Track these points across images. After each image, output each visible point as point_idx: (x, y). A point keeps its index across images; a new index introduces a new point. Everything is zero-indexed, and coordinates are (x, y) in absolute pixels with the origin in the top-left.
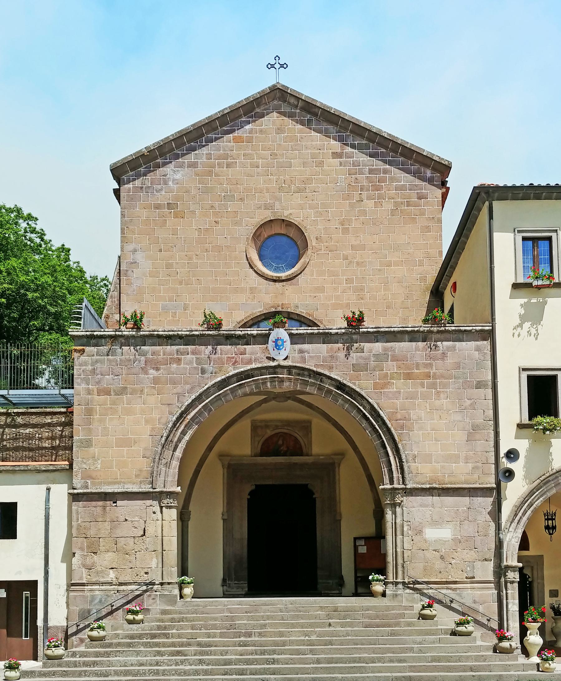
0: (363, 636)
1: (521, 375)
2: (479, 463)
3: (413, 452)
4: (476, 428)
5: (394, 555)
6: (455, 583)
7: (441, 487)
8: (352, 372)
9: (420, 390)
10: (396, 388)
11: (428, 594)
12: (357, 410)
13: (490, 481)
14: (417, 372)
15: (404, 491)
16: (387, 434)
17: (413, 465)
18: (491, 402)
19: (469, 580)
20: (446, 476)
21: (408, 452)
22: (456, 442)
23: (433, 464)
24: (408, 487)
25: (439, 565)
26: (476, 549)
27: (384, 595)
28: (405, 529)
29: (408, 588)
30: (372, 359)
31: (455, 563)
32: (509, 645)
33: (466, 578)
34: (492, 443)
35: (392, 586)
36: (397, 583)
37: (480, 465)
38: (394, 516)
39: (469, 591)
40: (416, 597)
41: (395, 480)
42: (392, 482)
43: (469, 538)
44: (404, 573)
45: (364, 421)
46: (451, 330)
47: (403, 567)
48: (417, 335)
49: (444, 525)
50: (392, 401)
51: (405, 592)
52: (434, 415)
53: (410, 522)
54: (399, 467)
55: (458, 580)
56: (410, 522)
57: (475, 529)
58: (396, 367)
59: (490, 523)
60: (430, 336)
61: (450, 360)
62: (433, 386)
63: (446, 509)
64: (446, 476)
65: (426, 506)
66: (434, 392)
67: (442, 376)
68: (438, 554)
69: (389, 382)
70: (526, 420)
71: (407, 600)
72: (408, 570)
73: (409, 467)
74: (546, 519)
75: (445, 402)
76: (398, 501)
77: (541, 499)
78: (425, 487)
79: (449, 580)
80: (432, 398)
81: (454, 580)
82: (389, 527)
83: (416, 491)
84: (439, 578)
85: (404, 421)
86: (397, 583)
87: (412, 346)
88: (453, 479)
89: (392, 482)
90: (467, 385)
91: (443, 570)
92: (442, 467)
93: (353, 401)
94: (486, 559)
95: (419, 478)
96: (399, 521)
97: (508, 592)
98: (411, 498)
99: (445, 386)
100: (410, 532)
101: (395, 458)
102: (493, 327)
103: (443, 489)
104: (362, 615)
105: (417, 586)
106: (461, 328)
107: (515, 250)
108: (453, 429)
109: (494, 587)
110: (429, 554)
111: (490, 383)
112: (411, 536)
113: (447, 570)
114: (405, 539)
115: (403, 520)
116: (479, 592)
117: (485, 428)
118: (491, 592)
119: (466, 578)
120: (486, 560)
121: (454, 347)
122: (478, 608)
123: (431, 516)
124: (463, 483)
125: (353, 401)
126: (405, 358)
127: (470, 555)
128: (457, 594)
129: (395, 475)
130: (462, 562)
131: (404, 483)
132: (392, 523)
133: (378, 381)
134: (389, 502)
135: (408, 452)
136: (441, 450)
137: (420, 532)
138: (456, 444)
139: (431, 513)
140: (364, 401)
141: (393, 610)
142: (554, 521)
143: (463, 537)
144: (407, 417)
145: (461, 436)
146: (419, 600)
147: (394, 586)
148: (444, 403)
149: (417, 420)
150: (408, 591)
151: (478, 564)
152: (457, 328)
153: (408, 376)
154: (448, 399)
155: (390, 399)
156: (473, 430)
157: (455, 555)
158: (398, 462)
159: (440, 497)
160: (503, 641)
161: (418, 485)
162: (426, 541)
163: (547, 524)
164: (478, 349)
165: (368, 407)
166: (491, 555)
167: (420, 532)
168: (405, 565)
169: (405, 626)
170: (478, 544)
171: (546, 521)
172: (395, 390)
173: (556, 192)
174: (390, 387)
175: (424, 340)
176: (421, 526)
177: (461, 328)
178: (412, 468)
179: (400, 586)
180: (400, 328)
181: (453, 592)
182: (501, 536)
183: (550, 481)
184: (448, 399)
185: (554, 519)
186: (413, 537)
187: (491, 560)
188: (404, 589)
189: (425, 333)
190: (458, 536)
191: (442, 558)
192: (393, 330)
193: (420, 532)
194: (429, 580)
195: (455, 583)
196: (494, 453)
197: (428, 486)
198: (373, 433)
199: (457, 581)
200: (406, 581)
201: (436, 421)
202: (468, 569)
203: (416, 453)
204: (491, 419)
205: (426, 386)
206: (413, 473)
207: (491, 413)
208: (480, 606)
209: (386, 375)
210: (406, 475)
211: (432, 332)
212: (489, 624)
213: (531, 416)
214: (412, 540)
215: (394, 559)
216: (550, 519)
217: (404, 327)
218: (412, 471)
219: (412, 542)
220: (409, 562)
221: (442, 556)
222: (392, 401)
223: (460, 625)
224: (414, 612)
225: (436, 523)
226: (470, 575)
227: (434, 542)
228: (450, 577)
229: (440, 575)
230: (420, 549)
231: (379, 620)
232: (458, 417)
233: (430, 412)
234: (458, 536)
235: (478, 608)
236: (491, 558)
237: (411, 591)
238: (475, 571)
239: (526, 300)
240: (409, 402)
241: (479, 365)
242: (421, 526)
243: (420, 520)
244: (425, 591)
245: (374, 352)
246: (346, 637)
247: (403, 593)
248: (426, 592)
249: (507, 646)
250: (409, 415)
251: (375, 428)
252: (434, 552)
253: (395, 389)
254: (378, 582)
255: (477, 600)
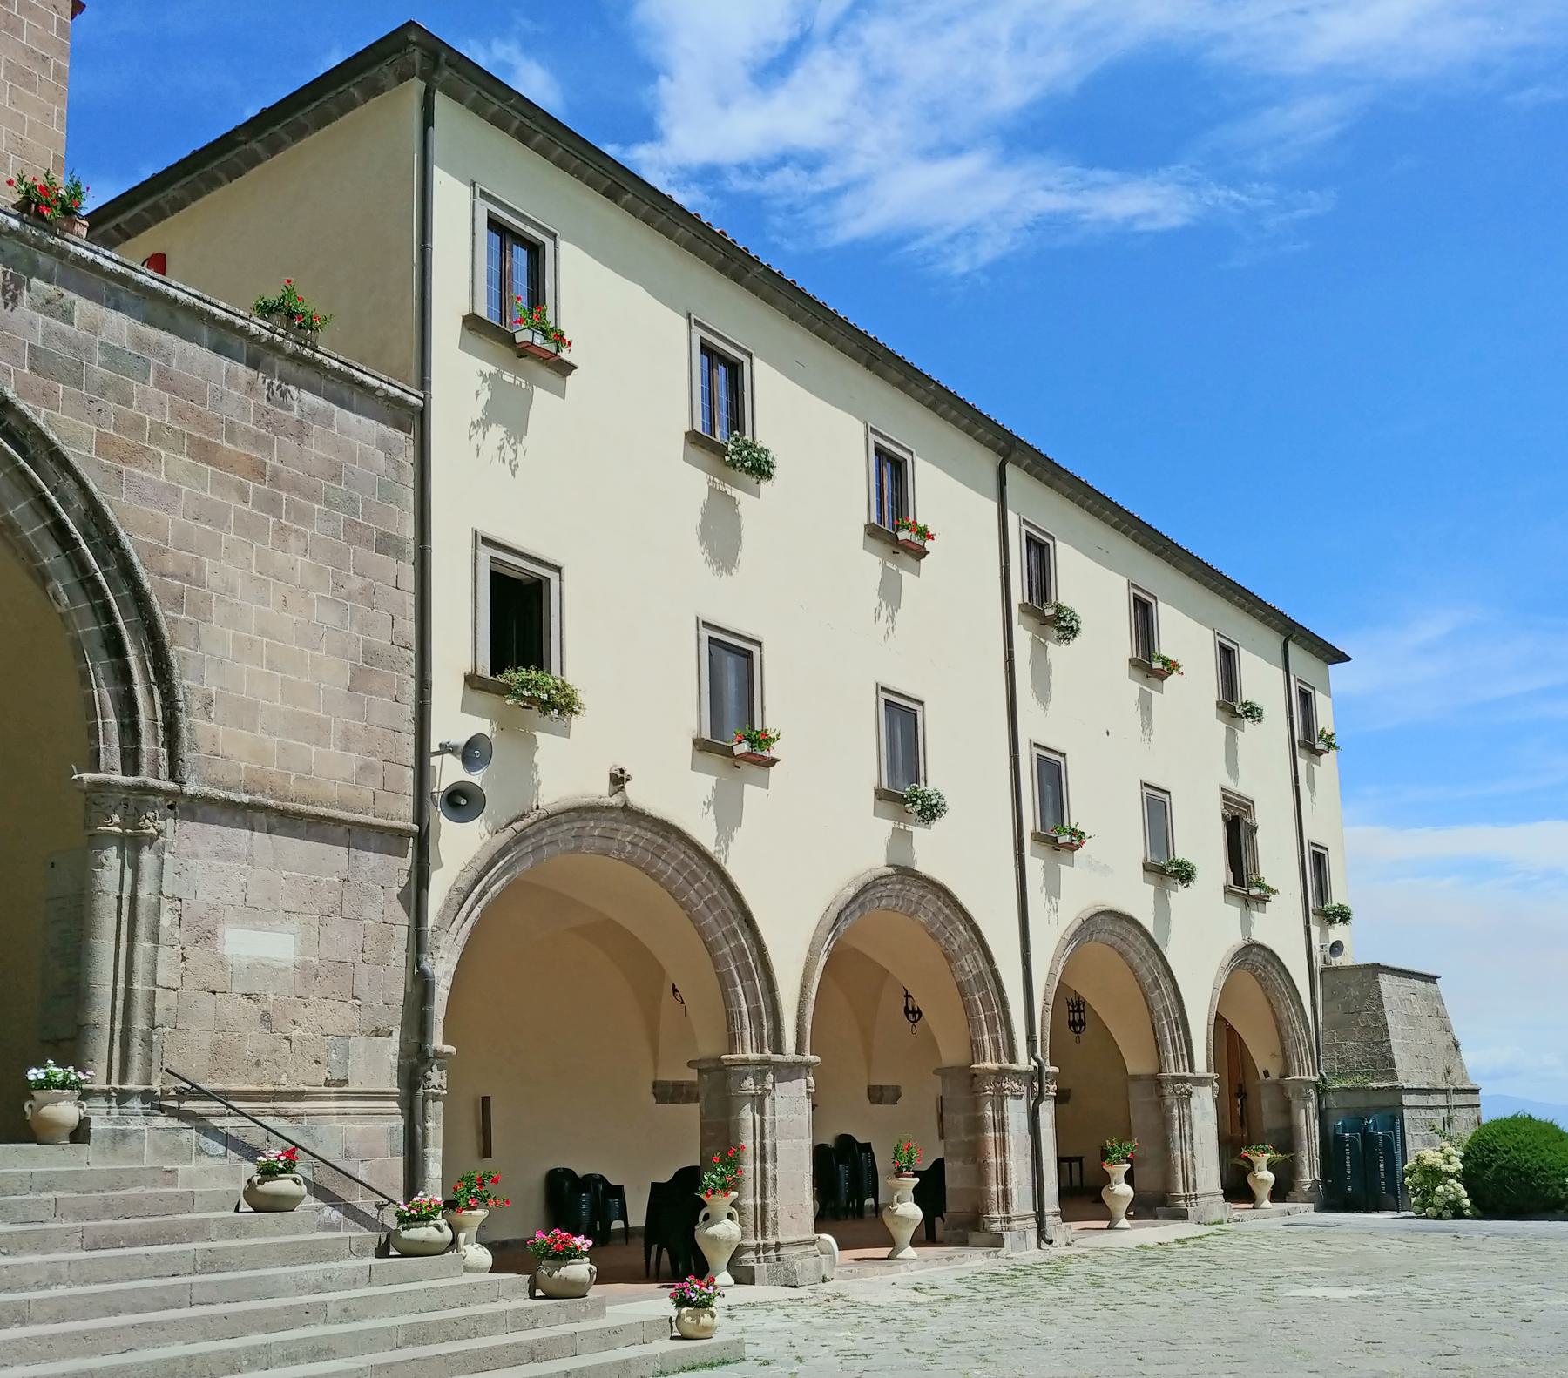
0: (110, 1281)
1: (478, 552)
2: (376, 756)
3: (205, 686)
4: (371, 656)
5: (119, 1003)
6: (298, 1096)
7: (281, 808)
8: (26, 370)
9: (234, 504)
10: (166, 475)
11: (221, 1130)
12: (30, 503)
13: (402, 813)
14: (230, 451)
15: (170, 802)
16: (133, 609)
17: (199, 722)
18: (410, 600)
19: (334, 1089)
20: (293, 778)
21: (190, 683)
22: (323, 685)
23: (258, 735)
24: (190, 789)
25: (255, 1040)
26: (357, 1001)
27: (80, 1134)
28: (166, 920)
29: (162, 1109)
30: (99, 356)
31: (302, 1039)
32: (588, 1273)
33: (328, 1083)
34: (409, 709)
35: (106, 1105)
36: (123, 1097)
37: (376, 761)
38: (128, 873)
39: (335, 1123)
40: (184, 1140)
41: (145, 761)
42: (131, 762)
43: (341, 966)
44: (148, 1062)
45: (54, 549)
46: (328, 366)
47: (148, 1042)
48: (235, 341)
49: (278, 922)
50: (154, 511)
51: (154, 1125)
52: (269, 590)
53: (180, 900)
54: (160, 723)
55: (307, 1089)
56: (180, 900)
57: (357, 943)
58: (170, 411)
59: (395, 930)
60: (269, 359)
61: (315, 450)
62: (272, 505)
63: (285, 873)
64: (293, 778)
65: (232, 857)
66: (271, 523)
67: (295, 487)
68: (255, 1006)
69: (147, 448)
70: (485, 669)
71: (157, 1150)
72: (165, 1055)
73: (190, 728)
74: (1070, 1011)
75: (299, 563)
76: (152, 830)
77: (504, 879)
78: (238, 800)
79: (283, 1088)
80: (268, 540)
81: (294, 1088)
82: (106, 910)
83: (206, 808)
84: (252, 1080)
85: (186, 585)
86: (123, 1097)
87: (219, 365)
88: (307, 789)
89: (131, 762)
90: (353, 531)
91: (266, 1056)
92: (284, 748)
93: (28, 468)
94: (377, 1030)
95: (217, 770)
96: (144, 893)
97: (428, 1125)
98: (189, 827)
99: (303, 516)
100: (177, 934)
101: (150, 692)
102: (426, 400)
103: (283, 813)
104: (52, 1207)
105: (188, 1105)
106: (356, 373)
107: (474, 234)
108: (317, 646)
109: (400, 1111)
110: (231, 1007)
111: (410, 548)
112: (179, 946)
113: (278, 1056)
114: (164, 953)
115: (161, 893)
116: (359, 1126)
117: (393, 665)
118: (388, 1125)
119: (328, 1083)
120: (377, 1033)
121: (327, 421)
122: (355, 1171)
123: (244, 888)
124: (332, 805)
125: (28, 468)
126: (194, 394)
127: (341, 1016)
128: (301, 1130)
129: (146, 745)
130: (319, 1035)
131: (173, 775)
132: (119, 898)
133: (112, 432)
134: (116, 829)
135: (190, 683)
136: (283, 698)
137: (207, 936)
138: (321, 692)
139: (243, 880)
140: (65, 479)
141: (135, 1183)
142: (1082, 1014)
143: (324, 962)
144: (194, 574)
145: (334, 673)
146: (194, 1150)
147: (114, 1104)
148: (297, 564)
149: (223, 592)
150: (161, 1121)
151: (359, 1044)
152: (344, 368)
153: (203, 451)
154: (308, 556)
155: (144, 499)
156: (367, 664)
157: (302, 1013)
158: (158, 706)
159: (273, 836)
160: (572, 1261)
161: (216, 791)
162: (222, 964)
163: (1071, 1019)
164: (384, 445)
165: (78, 503)
166: (394, 1019)
167: (209, 935)
168: (155, 1037)
169: (220, 1237)
170: (362, 986)
171: (1071, 1014)
172: (163, 478)
173: (564, 149)
174: (150, 465)
175: (253, 364)
176: (212, 918)
177: (356, 373)
178: (199, 734)
179: (136, 1104)
180: (195, 300)
181: (291, 1125)
182: (426, 965)
183: (528, 837)
184: (308, 556)
185: (1083, 1011)
186: (188, 948)
187: (391, 1034)
188: (146, 1114)
189: (259, 343)
190: (312, 959)
191: (266, 1019)
192: (173, 295)
193: (209, 935)
194: (226, 1087)
195: (298, 1096)
196: (413, 737)
197: (246, 799)
198: (79, 593)
199: (303, 1093)
200: (156, 1086)
201: (271, 609)
202: (334, 1056)
203: (214, 693)
204: (408, 645)
205: (251, 498)
206: (202, 750)
207: (409, 628)
208: (360, 1165)
209: (138, 425)
210: (187, 755)
211: (276, 348)
212: (381, 1218)
213: (497, 666)
214: (184, 959)
215: (119, 1014)
216: (1076, 1011)
217: (205, 301)
218: (200, 743)
219: (182, 965)
220: (168, 1029)
221: (266, 1013)
222: (154, 511)
223: (418, 1224)
224: (179, 1189)
225: (254, 913)
226: (338, 1075)
227: (246, 971)
228: (283, 1080)
229: (256, 1072)
230: (204, 989)
231: (110, 1222)
232: (331, 617)
233: (259, 578)
234: (312, 959)
235: (355, 1171)
236: (391, 1028)
237: (173, 1122)
238: (350, 1063)
239: (493, 369)
240: (203, 529)
241: (387, 490)
242: (212, 918)
243: (210, 899)
244: (216, 1122)
245: (104, 337)
246: (47, 1287)
247: (146, 1128)
248: (217, 1124)
249: (583, 1276)
250: (200, 569)
251: (94, 580)
252: (244, 1001)
253: (163, 475)
254: (67, 1092)
255: (354, 1148)
